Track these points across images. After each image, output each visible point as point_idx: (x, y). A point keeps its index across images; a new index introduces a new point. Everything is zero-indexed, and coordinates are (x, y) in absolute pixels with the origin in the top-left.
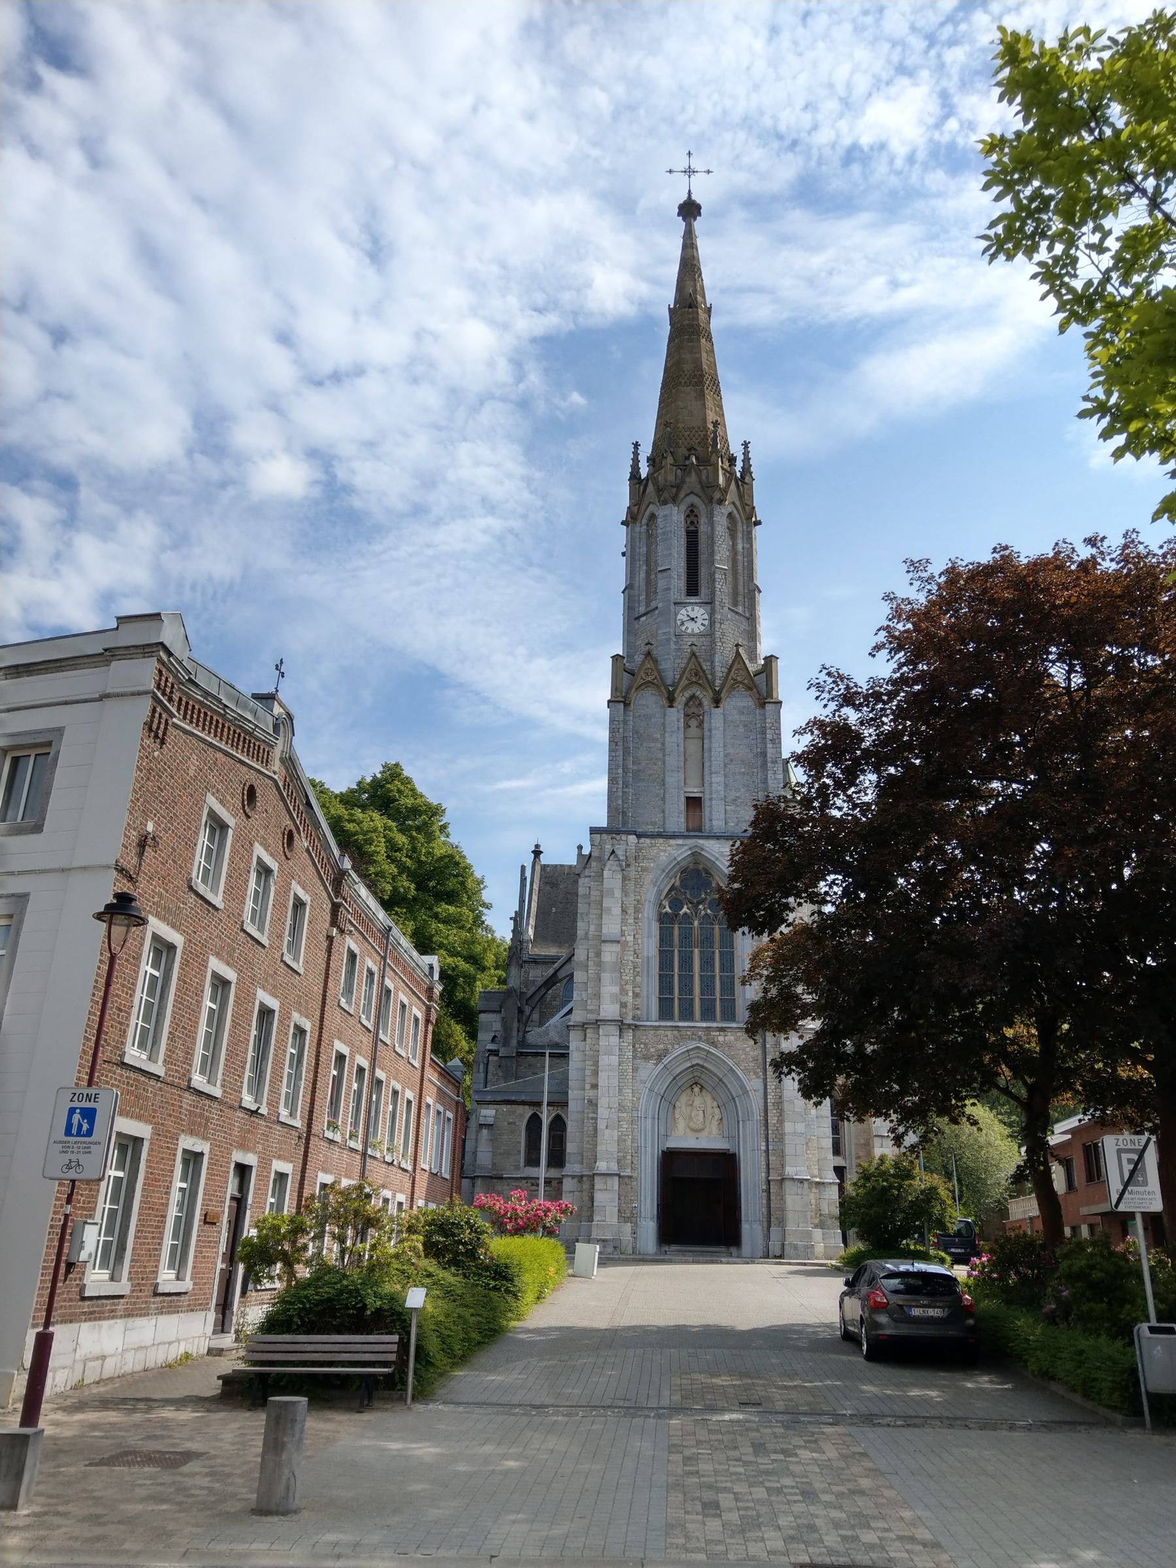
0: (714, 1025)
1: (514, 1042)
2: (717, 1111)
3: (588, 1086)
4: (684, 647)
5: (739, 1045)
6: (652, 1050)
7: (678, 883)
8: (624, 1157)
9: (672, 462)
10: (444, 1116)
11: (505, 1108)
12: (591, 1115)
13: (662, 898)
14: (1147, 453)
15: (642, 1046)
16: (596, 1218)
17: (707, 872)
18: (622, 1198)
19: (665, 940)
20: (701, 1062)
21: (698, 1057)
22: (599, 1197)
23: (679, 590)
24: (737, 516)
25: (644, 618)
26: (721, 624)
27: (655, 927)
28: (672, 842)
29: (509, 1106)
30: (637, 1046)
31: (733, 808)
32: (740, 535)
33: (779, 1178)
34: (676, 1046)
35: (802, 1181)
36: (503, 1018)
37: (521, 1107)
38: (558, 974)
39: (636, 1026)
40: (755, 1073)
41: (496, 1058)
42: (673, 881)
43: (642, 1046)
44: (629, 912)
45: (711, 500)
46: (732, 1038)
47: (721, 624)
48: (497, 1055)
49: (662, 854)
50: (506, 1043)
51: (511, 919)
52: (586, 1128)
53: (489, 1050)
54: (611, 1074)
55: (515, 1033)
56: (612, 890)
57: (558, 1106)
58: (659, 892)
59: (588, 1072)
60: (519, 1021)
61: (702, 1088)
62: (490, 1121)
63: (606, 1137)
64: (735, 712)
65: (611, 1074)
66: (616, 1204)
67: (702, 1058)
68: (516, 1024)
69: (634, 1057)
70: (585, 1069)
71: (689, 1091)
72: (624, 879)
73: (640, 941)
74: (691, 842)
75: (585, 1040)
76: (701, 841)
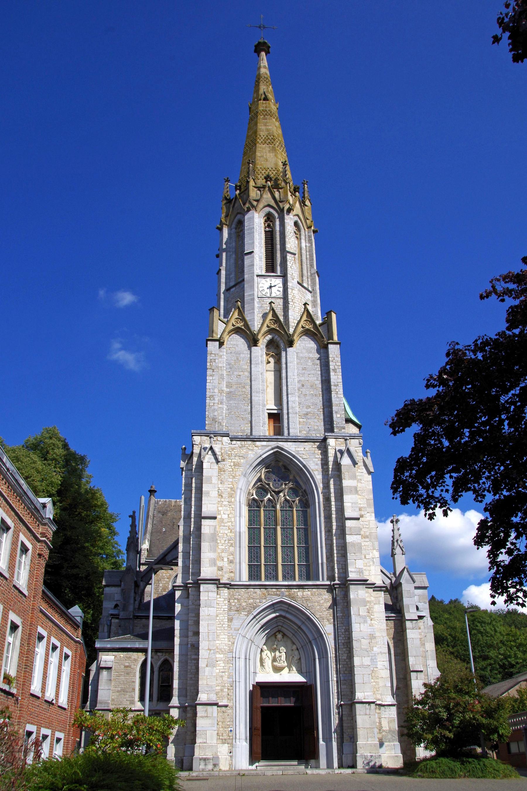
0: (294, 583)
1: (131, 608)
2: (296, 652)
3: (190, 634)
4: (265, 306)
5: (315, 598)
6: (244, 604)
7: (263, 477)
8: (222, 690)
9: (254, 185)
10: (61, 651)
11: (122, 655)
12: (193, 657)
13: (250, 488)
14: (414, 446)
15: (236, 601)
16: (198, 740)
17: (286, 468)
18: (220, 723)
19: (253, 519)
20: (283, 614)
21: (281, 610)
22: (201, 723)
23: (261, 268)
24: (301, 224)
25: (234, 289)
26: (292, 289)
27: (245, 510)
28: (258, 443)
29: (125, 653)
30: (231, 601)
31: (305, 420)
32: (303, 237)
33: (350, 702)
34: (264, 601)
35: (369, 703)
36: (122, 590)
37: (135, 654)
38: (167, 558)
39: (231, 585)
40: (328, 620)
41: (117, 621)
42: (259, 475)
43: (236, 601)
44: (224, 495)
45: (282, 210)
46: (309, 593)
47: (292, 289)
48: (118, 618)
49: (250, 452)
50: (125, 608)
51: (130, 516)
52: (189, 667)
53: (112, 615)
54: (210, 622)
55: (132, 601)
56: (211, 477)
57: (166, 652)
58: (248, 483)
59: (190, 622)
60: (135, 593)
61: (284, 635)
62: (109, 665)
63: (206, 674)
64: (304, 351)
65: (210, 622)
66: (215, 728)
67: (284, 611)
68: (132, 594)
69: (230, 609)
70: (188, 621)
71: (273, 638)
72: (220, 470)
73: (233, 520)
74: (273, 444)
75: (188, 597)
76: (281, 444)
